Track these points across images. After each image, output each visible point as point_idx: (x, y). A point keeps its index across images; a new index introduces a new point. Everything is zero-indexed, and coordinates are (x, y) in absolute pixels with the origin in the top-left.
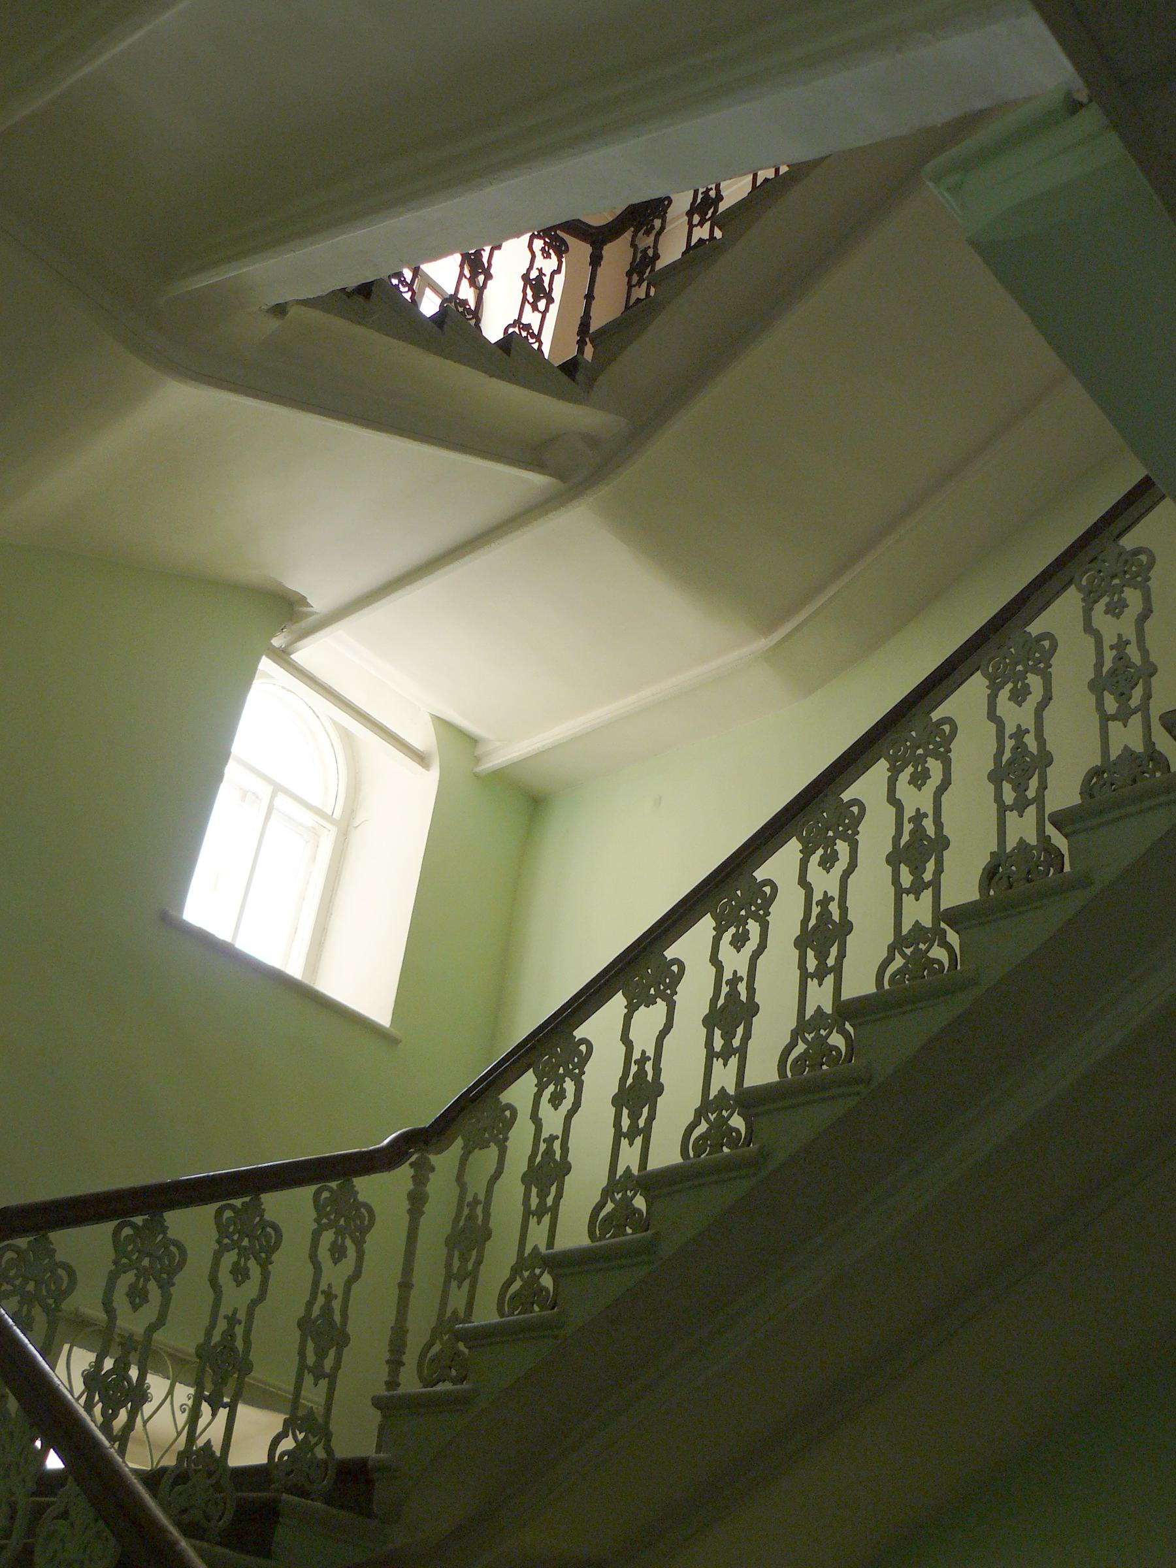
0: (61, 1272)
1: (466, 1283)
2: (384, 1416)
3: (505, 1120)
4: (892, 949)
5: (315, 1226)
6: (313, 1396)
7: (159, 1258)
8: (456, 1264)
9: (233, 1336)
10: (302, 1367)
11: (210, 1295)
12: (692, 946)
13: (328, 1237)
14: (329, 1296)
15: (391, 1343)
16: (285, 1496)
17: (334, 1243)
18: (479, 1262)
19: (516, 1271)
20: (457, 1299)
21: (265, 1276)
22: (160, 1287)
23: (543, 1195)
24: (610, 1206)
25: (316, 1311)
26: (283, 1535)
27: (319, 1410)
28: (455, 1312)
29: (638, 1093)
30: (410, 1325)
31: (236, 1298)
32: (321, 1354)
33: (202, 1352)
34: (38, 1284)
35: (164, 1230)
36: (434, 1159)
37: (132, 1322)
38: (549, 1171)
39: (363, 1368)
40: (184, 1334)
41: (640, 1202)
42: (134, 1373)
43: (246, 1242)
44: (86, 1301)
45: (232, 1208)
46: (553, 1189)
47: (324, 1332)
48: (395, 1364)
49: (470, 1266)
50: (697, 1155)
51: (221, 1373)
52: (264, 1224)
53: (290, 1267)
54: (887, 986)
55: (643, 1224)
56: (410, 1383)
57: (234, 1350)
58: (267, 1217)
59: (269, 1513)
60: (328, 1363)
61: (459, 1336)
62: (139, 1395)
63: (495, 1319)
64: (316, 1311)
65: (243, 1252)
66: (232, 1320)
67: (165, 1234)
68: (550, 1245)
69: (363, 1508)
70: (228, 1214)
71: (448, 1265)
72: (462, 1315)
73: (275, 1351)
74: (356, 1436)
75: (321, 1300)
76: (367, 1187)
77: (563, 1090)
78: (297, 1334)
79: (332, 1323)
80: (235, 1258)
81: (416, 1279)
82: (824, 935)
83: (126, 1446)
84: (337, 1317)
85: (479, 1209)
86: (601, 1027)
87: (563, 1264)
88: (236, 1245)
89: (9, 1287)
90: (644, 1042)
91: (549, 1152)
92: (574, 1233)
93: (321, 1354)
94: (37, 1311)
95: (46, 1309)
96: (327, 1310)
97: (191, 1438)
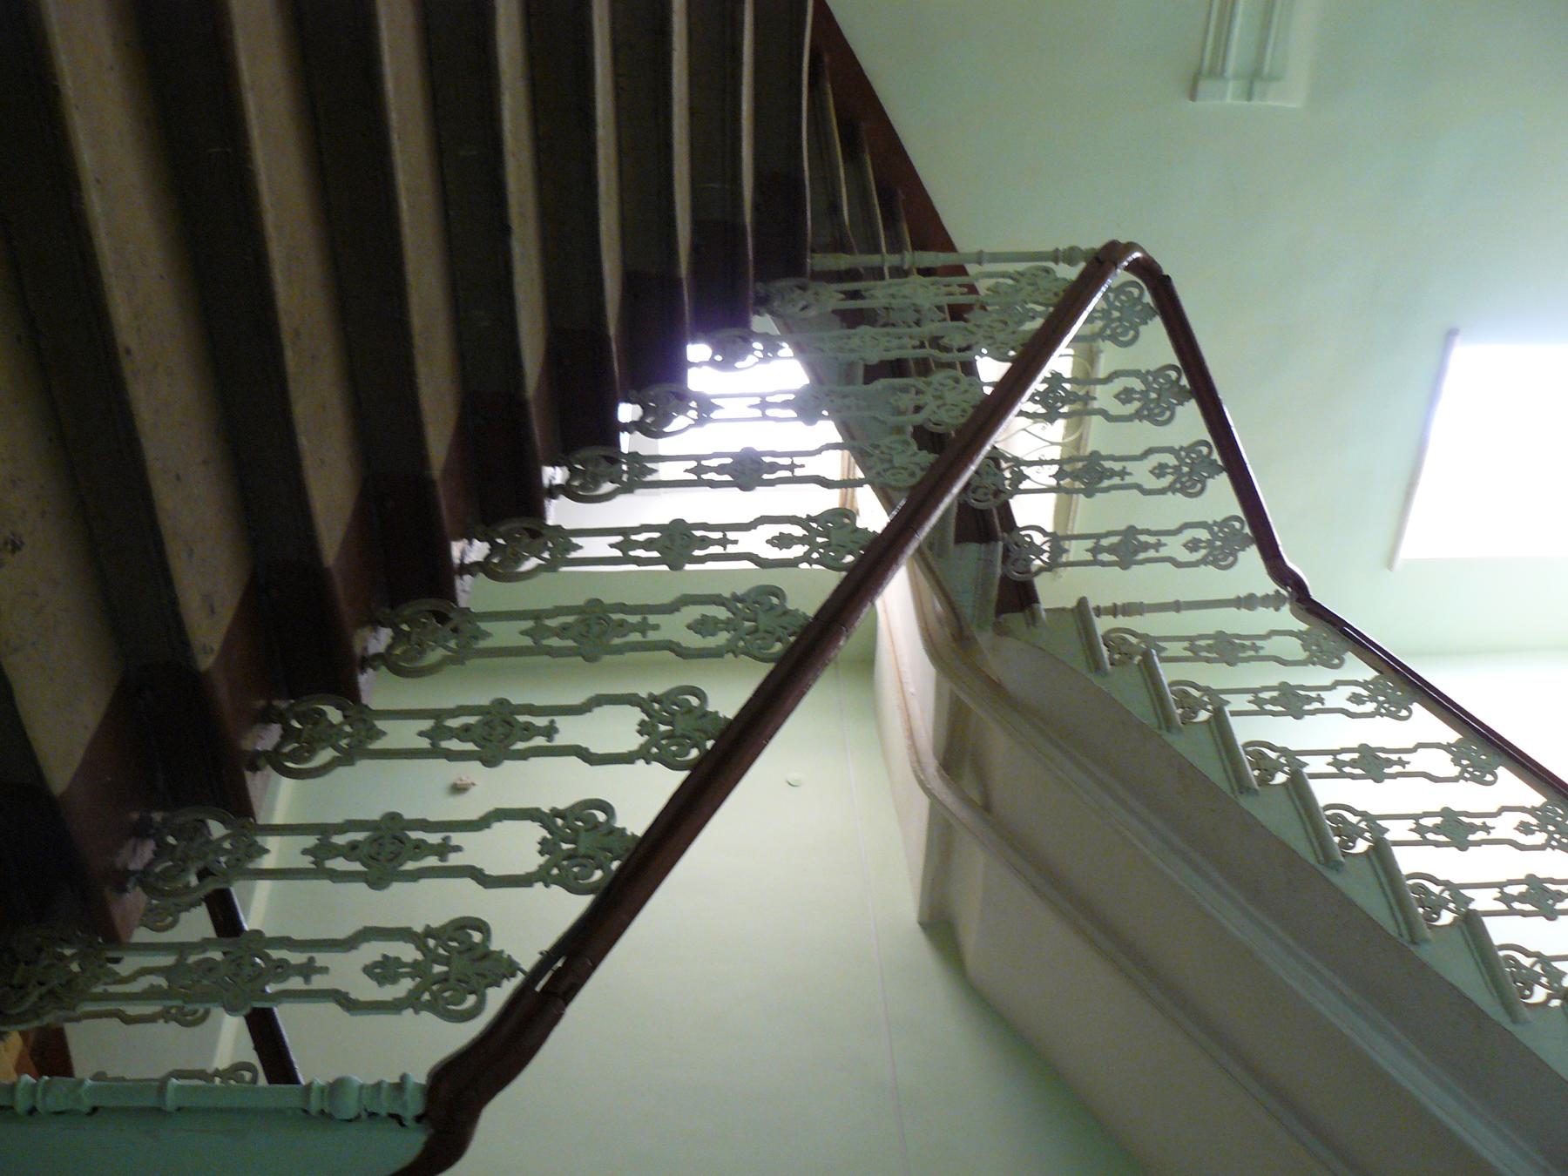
0: (1132, 333)
1: (1188, 654)
2: (1072, 610)
3: (1328, 659)
4: (1538, 955)
6: (1077, 550)
7: (1158, 406)
8: (1203, 643)
9: (1110, 477)
10: (1098, 537)
11: (1138, 451)
12: (1510, 788)
13: (1204, 535)
15: (1129, 604)
16: (1001, 544)
17: (1200, 541)
18: (1208, 660)
19: (1206, 690)
20: (1175, 649)
21: (1162, 491)
23: (1273, 701)
24: (1273, 755)
25: (1143, 538)
26: (973, 549)
27: (1070, 557)
28: (1164, 649)
29: (1372, 764)
30: (1148, 615)
31: (1141, 472)
32: (1111, 550)
33: (1095, 457)
34: (1119, 319)
35: (1181, 403)
36: (1286, 609)
37: (1104, 396)
38: (1293, 702)
39: (1104, 586)
40: (1100, 437)
41: (1280, 778)
42: (1065, 410)
43: (1186, 469)
44: (1110, 357)
46: (1280, 709)
47: (1128, 548)
48: (1114, 611)
49: (1204, 654)
50: (1328, 818)
51: (1083, 474)
53: (1174, 509)
54: (1502, 953)
55: (1264, 781)
56: (1102, 625)
57: (1101, 480)
60: (1105, 557)
61: (1146, 655)
62: (1050, 417)
63: (1166, 682)
64: (1143, 538)
65: (1177, 469)
66: (1123, 474)
68: (1234, 713)
69: (1003, 607)
70: (1205, 450)
71: (1201, 637)
72: (1163, 654)
73: (1102, 513)
74: (1053, 592)
75: (1152, 540)
76: (1251, 557)
77: (1363, 703)
78: (1122, 527)
79: (1136, 552)
81: (1185, 614)
82: (1456, 830)
83: (333, 825)
84: (1142, 556)
85: (1252, 653)
86: (1423, 724)
87: (1220, 726)
90: (1417, 762)
91: (1309, 700)
92: (1245, 731)
93: (1111, 550)
94: (1099, 324)
96: (1146, 547)
97: (1030, 464)
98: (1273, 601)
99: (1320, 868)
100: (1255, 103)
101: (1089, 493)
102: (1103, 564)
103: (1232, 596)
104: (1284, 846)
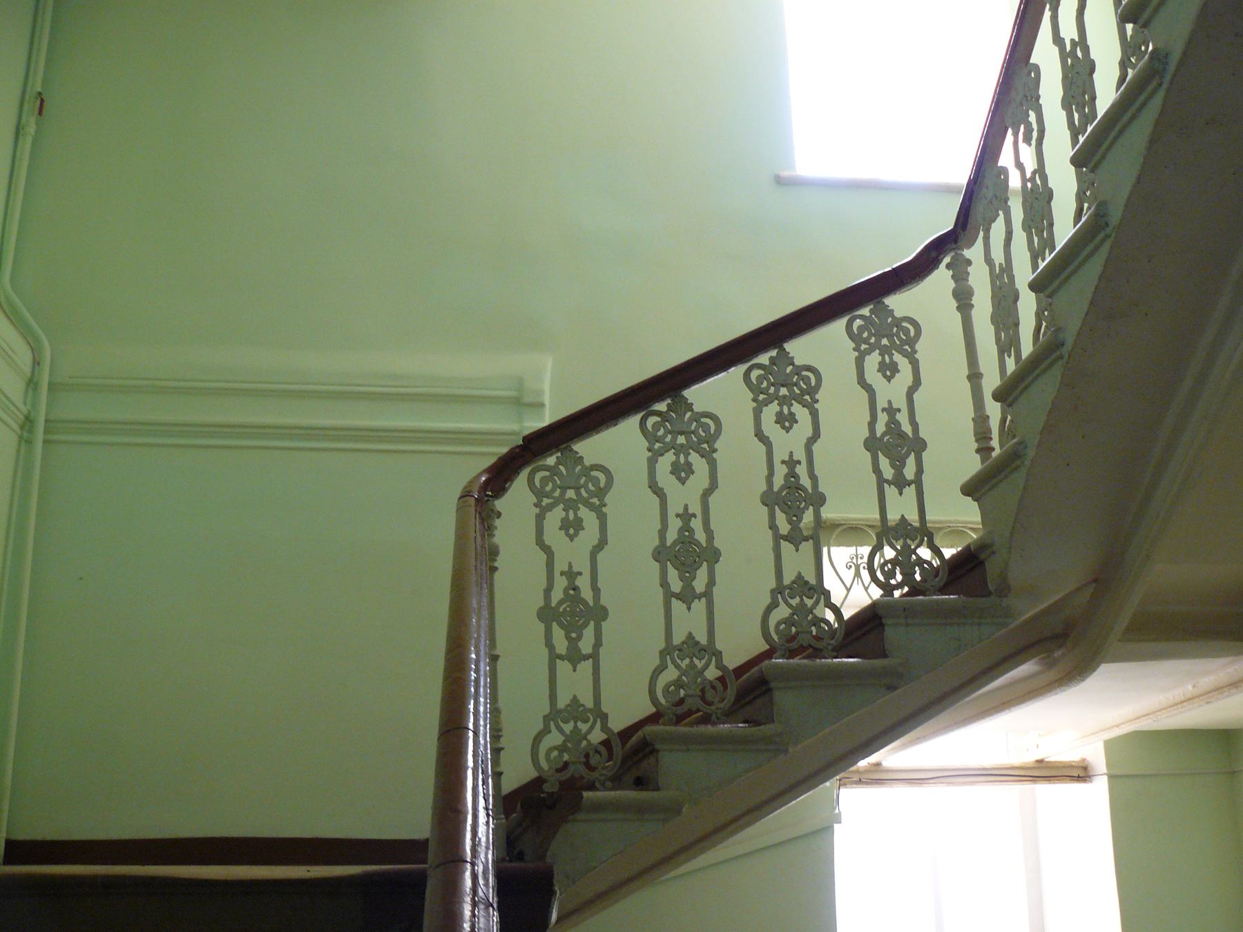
5: (537, 510)
10: (881, 481)
14: (571, 575)
22: (702, 456)
31: (684, 496)
32: (898, 464)
35: (689, 407)
36: (967, 253)
45: (759, 366)
47: (896, 446)
52: (798, 370)
58: (797, 362)
59: (646, 749)
66: (686, 516)
67: (793, 364)
75: (882, 418)
79: (902, 435)
80: (674, 458)
88: (877, 346)
89: (550, 501)
93: (898, 464)
95: (591, 507)
96: (893, 425)
98: (960, 271)
99: (1168, 78)
100: (547, 400)
101: (818, 500)
102: (920, 471)
103: (958, 316)
104: (1153, 141)
